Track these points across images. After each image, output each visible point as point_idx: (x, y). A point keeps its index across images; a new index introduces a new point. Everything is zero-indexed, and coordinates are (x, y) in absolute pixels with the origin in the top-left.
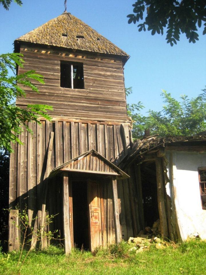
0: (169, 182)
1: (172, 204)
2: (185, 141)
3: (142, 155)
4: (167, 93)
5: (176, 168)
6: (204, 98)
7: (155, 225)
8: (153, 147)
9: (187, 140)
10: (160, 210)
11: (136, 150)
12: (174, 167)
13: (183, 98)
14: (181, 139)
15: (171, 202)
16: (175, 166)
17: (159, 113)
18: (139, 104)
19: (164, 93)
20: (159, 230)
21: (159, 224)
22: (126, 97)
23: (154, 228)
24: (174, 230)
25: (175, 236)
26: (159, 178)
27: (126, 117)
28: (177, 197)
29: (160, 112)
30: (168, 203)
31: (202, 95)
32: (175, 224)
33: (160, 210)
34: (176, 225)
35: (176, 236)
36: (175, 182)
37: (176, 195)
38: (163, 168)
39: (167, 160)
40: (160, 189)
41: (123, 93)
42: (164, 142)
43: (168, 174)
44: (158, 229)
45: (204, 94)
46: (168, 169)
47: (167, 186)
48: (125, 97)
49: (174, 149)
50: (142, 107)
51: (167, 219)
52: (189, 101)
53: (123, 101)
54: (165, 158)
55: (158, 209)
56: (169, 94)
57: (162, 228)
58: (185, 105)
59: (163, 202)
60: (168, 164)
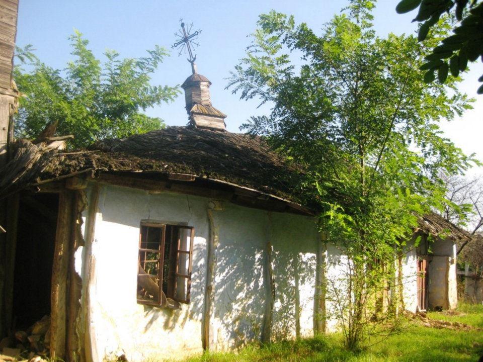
0: (83, 245)
1: (82, 291)
2: (137, 171)
3: (40, 186)
4: (83, 38)
5: (102, 218)
6: (148, 66)
7: (38, 328)
8: (69, 172)
9: (141, 171)
10: (55, 302)
11: (24, 169)
12: (99, 216)
13: (109, 56)
14: (128, 165)
15: (80, 287)
16: (101, 214)
17: (56, 72)
18: (26, 48)
19: (76, 37)
20: (46, 340)
21: (48, 326)
22: (15, 38)
23: (34, 335)
24: (80, 345)
25: (79, 356)
26: (63, 232)
27: (8, 82)
28: (95, 279)
29: (58, 70)
30: (75, 288)
31: (145, 59)
32: (84, 332)
33: (54, 300)
34: (84, 334)
35: (81, 357)
36: (95, 248)
37: (93, 275)
38: (75, 214)
39: (86, 199)
40: (61, 256)
41: (12, 26)
42: (95, 166)
43: (83, 227)
44: (42, 336)
45: (149, 60)
46: (84, 219)
47: (78, 254)
48: (13, 37)
49: (106, 180)
50: (32, 58)
51: (67, 321)
52: (118, 64)
53: (8, 43)
54: (83, 193)
55: (50, 297)
56: (86, 43)
57: (55, 339)
58: (110, 69)
59: (64, 285)
60: (86, 208)
